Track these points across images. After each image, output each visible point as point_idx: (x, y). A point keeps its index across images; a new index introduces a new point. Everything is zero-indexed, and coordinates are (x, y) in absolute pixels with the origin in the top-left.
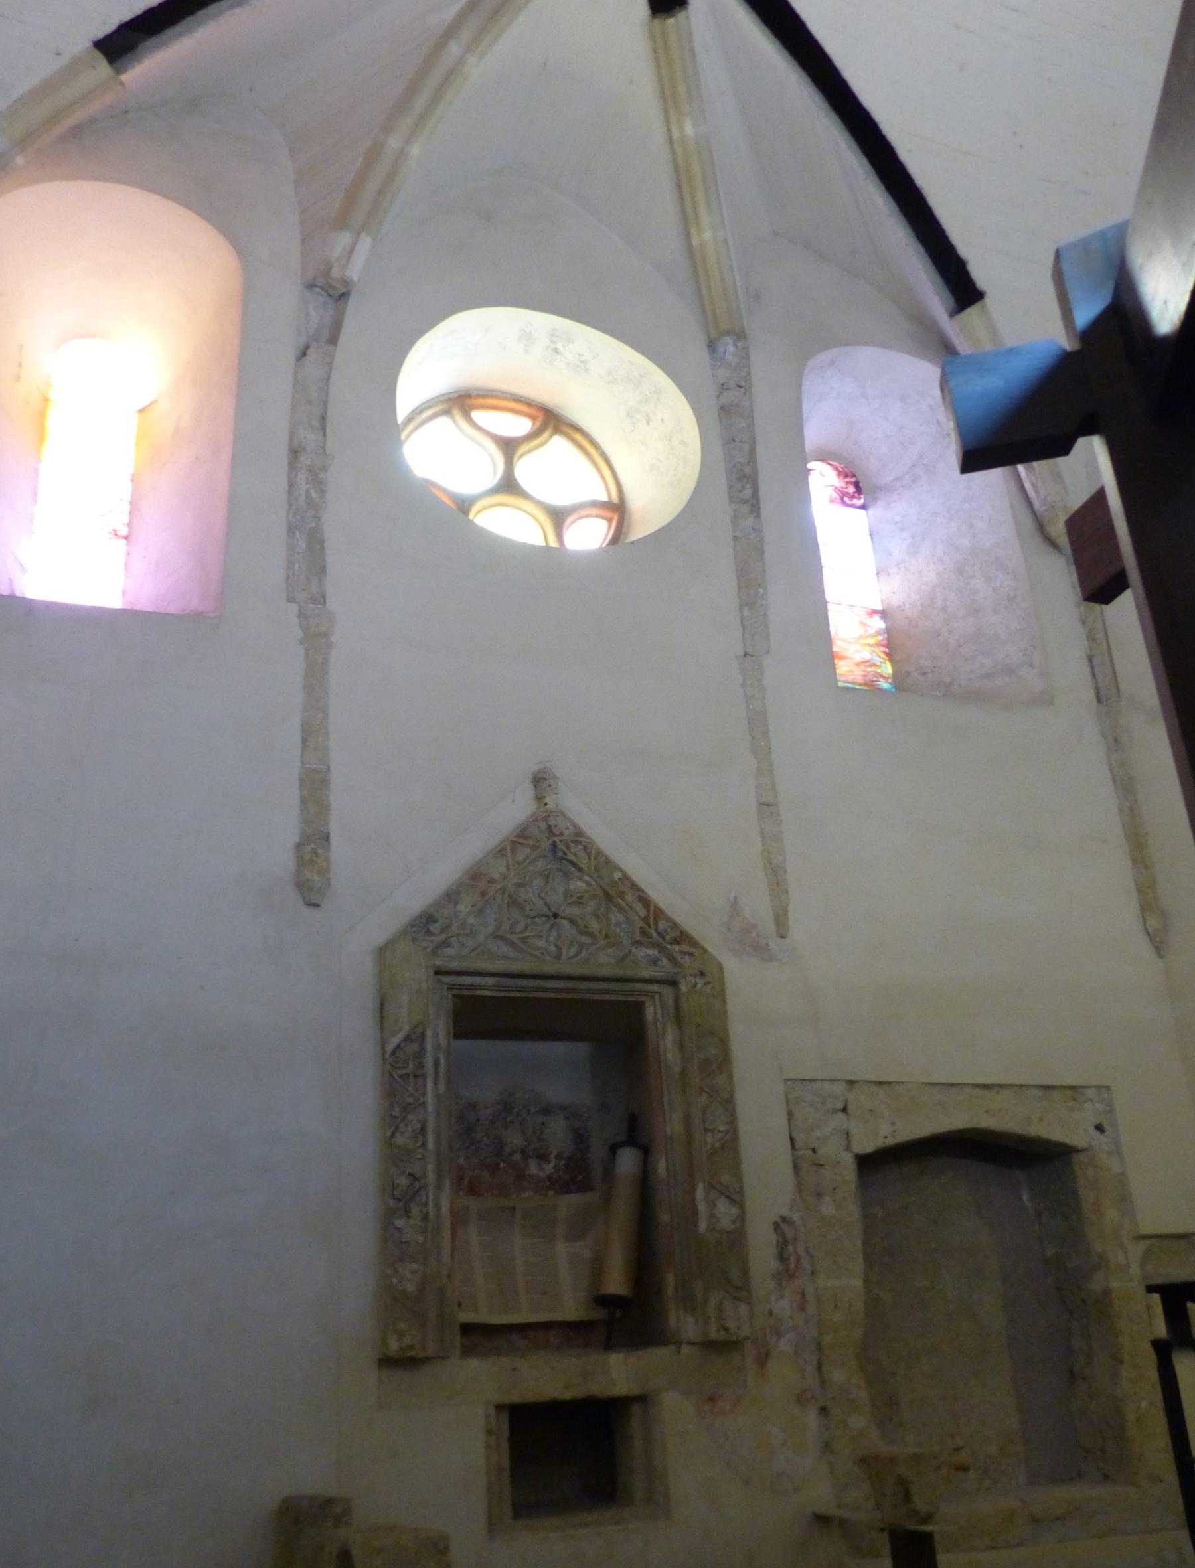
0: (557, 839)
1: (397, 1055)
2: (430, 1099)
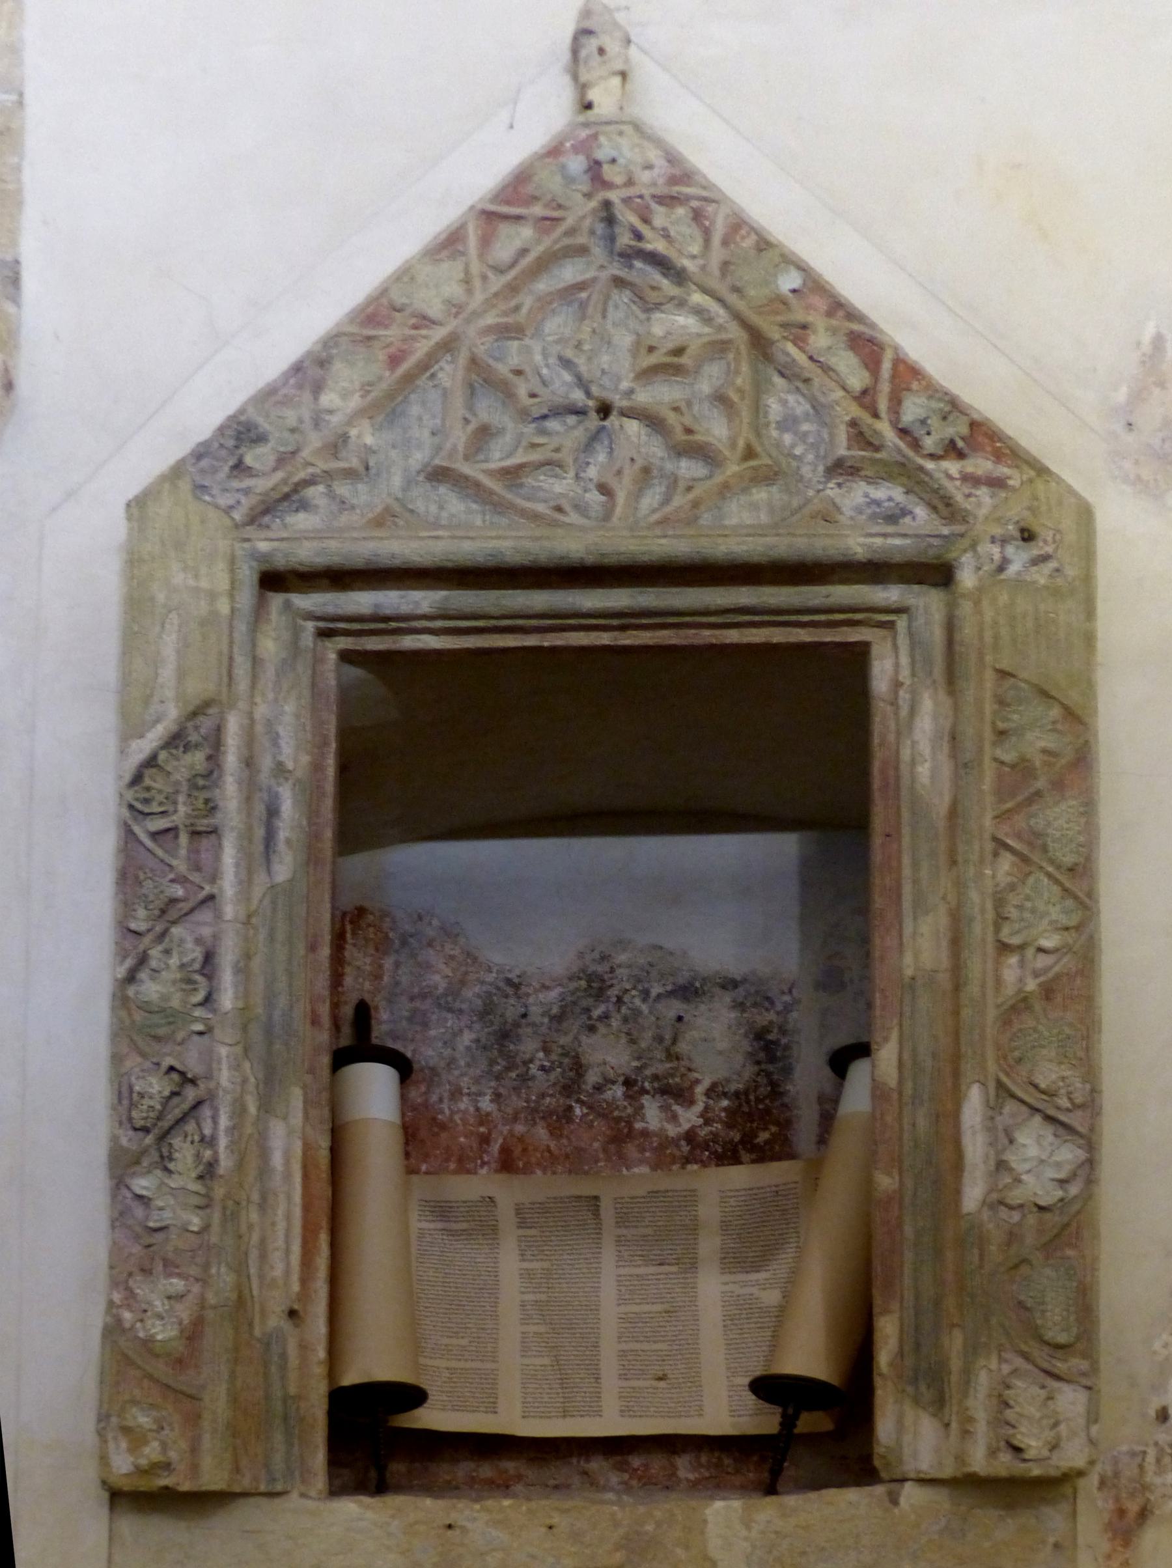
0: (614, 196)
1: (147, 782)
2: (228, 886)
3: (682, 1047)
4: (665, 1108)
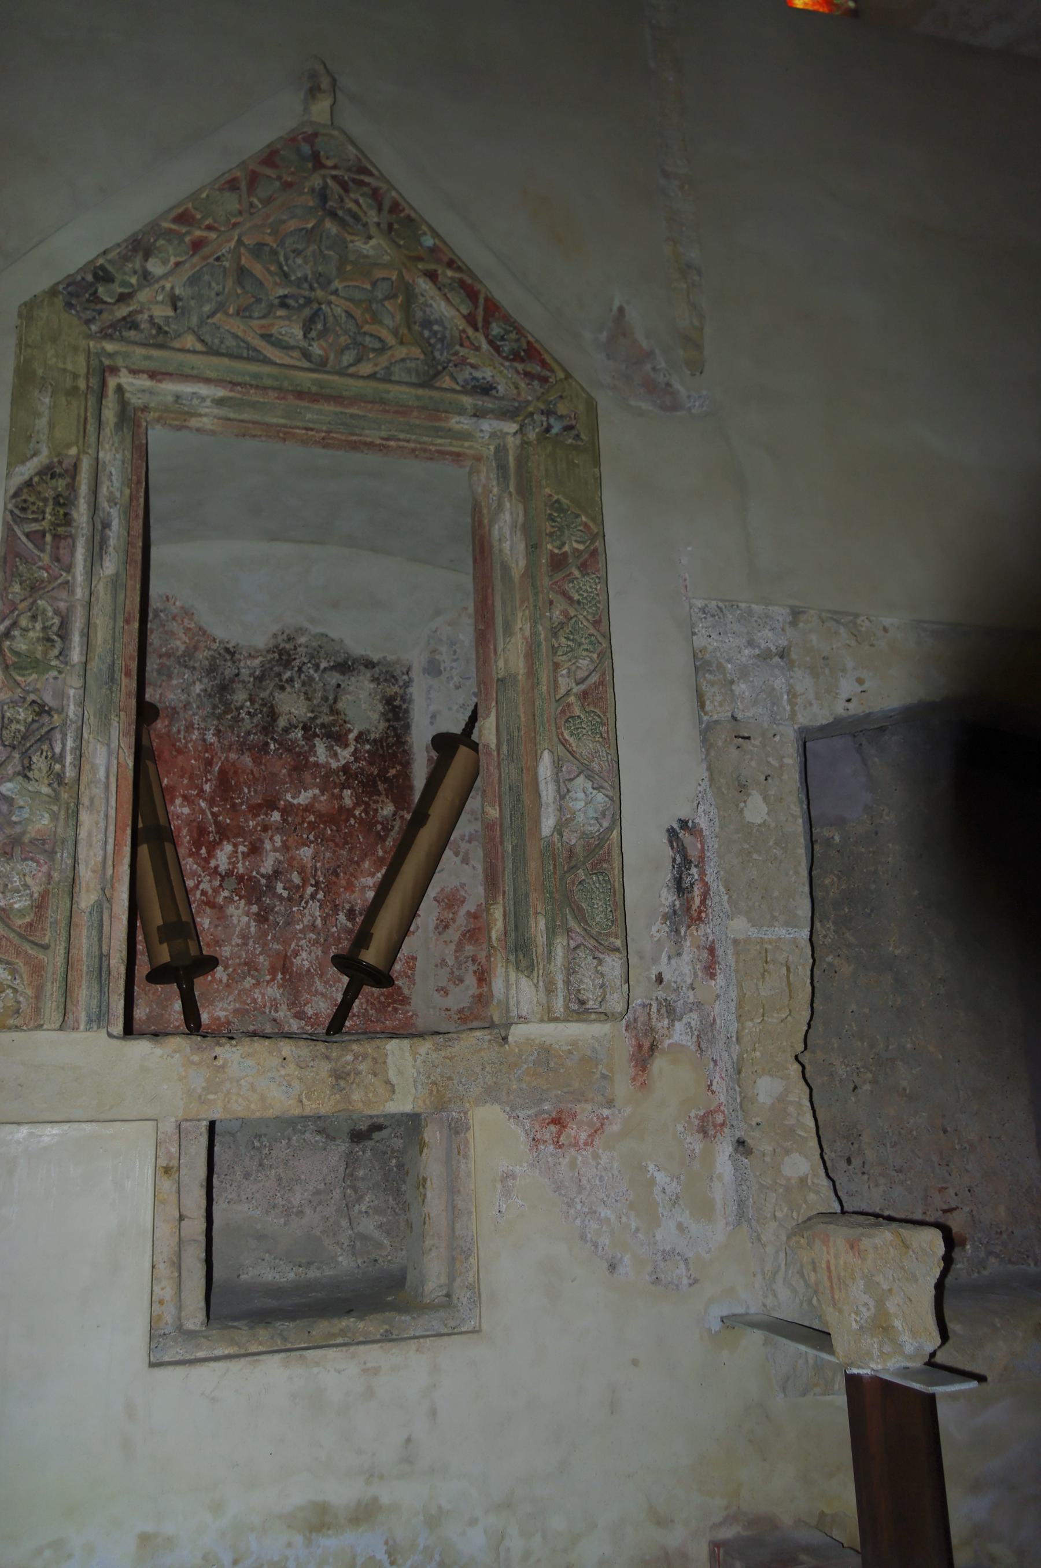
3: (340, 705)
4: (329, 748)
